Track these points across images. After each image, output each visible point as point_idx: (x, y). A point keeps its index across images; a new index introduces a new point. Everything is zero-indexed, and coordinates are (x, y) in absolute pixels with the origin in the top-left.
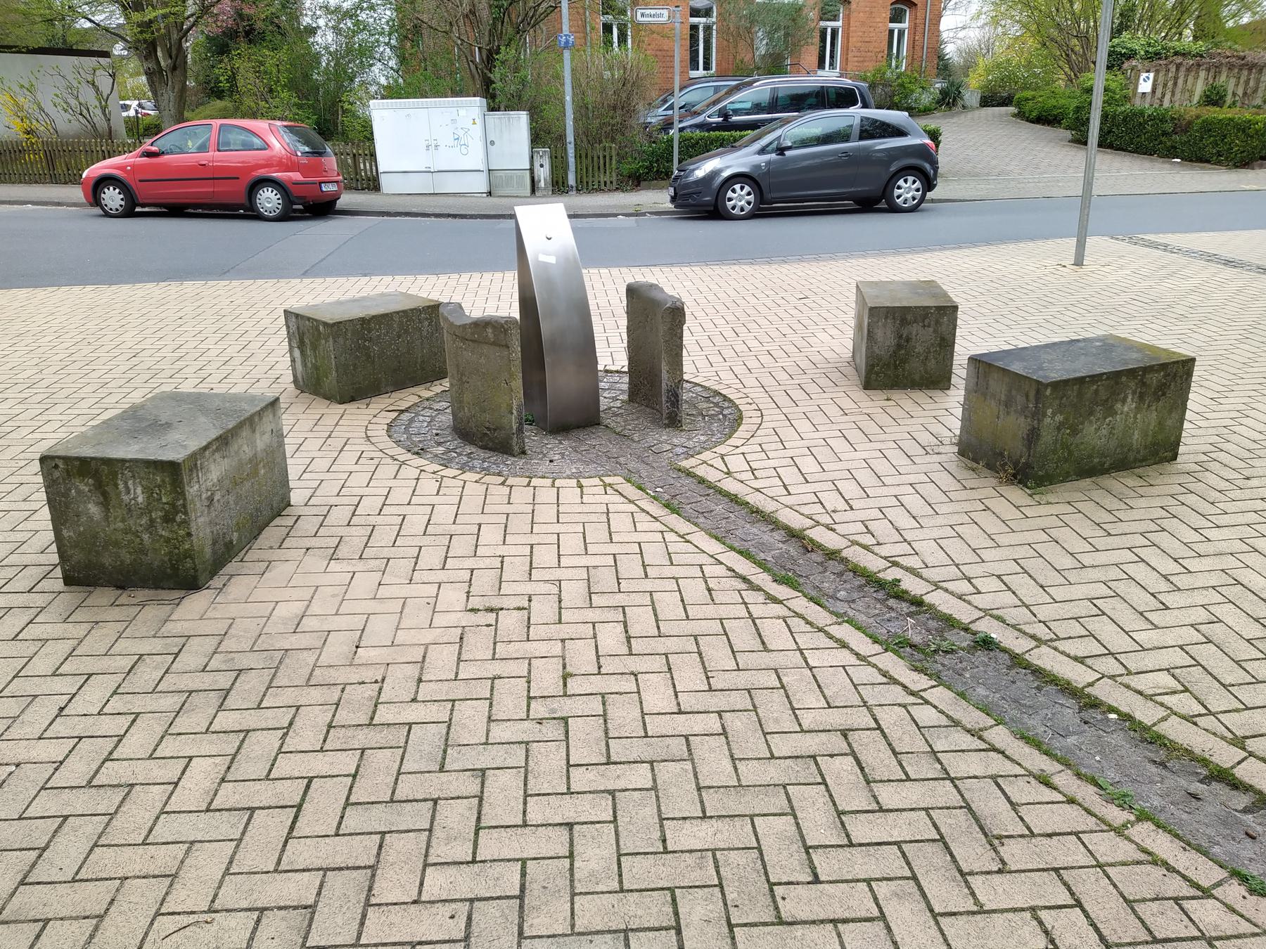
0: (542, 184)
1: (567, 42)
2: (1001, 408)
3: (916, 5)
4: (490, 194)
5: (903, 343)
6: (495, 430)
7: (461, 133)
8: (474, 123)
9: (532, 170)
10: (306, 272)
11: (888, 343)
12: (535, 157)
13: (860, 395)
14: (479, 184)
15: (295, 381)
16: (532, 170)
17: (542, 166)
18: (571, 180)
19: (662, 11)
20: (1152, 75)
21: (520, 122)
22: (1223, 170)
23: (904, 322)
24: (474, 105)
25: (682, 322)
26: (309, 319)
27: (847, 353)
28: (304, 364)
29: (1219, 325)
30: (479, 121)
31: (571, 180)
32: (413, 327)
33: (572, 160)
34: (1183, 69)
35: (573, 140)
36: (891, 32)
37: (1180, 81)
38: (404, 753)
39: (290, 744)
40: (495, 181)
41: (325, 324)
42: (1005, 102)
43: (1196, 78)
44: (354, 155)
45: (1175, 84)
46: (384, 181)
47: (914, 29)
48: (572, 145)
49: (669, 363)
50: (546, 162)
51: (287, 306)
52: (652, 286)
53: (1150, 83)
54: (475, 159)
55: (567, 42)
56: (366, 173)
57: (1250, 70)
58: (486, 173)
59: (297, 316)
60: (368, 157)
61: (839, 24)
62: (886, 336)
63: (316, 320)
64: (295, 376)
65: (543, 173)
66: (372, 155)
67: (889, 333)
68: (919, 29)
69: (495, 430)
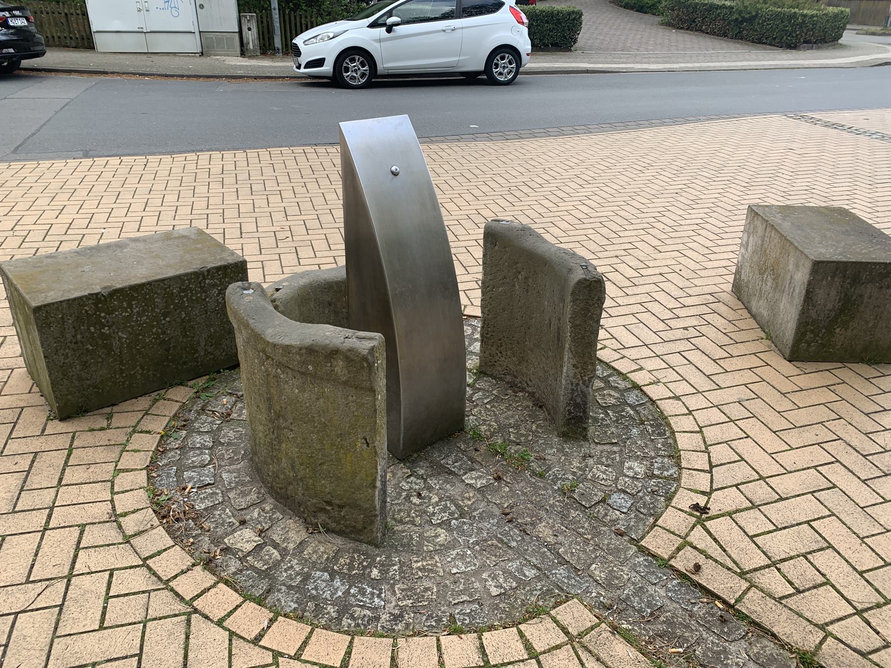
6: (341, 507)
10: (17, 148)
12: (243, 21)
13: (788, 368)
14: (192, 44)
17: (249, 29)
22: (780, 50)
23: (855, 280)
29: (703, 145)
32: (190, 300)
33: (277, 24)
44: (66, 14)
46: (97, 38)
48: (277, 11)
49: (575, 354)
50: (254, 25)
52: (525, 229)
56: (79, 31)
58: (197, 34)
60: (80, 17)
62: (828, 298)
65: (252, 36)
66: (84, 15)
67: (833, 293)
69: (341, 507)
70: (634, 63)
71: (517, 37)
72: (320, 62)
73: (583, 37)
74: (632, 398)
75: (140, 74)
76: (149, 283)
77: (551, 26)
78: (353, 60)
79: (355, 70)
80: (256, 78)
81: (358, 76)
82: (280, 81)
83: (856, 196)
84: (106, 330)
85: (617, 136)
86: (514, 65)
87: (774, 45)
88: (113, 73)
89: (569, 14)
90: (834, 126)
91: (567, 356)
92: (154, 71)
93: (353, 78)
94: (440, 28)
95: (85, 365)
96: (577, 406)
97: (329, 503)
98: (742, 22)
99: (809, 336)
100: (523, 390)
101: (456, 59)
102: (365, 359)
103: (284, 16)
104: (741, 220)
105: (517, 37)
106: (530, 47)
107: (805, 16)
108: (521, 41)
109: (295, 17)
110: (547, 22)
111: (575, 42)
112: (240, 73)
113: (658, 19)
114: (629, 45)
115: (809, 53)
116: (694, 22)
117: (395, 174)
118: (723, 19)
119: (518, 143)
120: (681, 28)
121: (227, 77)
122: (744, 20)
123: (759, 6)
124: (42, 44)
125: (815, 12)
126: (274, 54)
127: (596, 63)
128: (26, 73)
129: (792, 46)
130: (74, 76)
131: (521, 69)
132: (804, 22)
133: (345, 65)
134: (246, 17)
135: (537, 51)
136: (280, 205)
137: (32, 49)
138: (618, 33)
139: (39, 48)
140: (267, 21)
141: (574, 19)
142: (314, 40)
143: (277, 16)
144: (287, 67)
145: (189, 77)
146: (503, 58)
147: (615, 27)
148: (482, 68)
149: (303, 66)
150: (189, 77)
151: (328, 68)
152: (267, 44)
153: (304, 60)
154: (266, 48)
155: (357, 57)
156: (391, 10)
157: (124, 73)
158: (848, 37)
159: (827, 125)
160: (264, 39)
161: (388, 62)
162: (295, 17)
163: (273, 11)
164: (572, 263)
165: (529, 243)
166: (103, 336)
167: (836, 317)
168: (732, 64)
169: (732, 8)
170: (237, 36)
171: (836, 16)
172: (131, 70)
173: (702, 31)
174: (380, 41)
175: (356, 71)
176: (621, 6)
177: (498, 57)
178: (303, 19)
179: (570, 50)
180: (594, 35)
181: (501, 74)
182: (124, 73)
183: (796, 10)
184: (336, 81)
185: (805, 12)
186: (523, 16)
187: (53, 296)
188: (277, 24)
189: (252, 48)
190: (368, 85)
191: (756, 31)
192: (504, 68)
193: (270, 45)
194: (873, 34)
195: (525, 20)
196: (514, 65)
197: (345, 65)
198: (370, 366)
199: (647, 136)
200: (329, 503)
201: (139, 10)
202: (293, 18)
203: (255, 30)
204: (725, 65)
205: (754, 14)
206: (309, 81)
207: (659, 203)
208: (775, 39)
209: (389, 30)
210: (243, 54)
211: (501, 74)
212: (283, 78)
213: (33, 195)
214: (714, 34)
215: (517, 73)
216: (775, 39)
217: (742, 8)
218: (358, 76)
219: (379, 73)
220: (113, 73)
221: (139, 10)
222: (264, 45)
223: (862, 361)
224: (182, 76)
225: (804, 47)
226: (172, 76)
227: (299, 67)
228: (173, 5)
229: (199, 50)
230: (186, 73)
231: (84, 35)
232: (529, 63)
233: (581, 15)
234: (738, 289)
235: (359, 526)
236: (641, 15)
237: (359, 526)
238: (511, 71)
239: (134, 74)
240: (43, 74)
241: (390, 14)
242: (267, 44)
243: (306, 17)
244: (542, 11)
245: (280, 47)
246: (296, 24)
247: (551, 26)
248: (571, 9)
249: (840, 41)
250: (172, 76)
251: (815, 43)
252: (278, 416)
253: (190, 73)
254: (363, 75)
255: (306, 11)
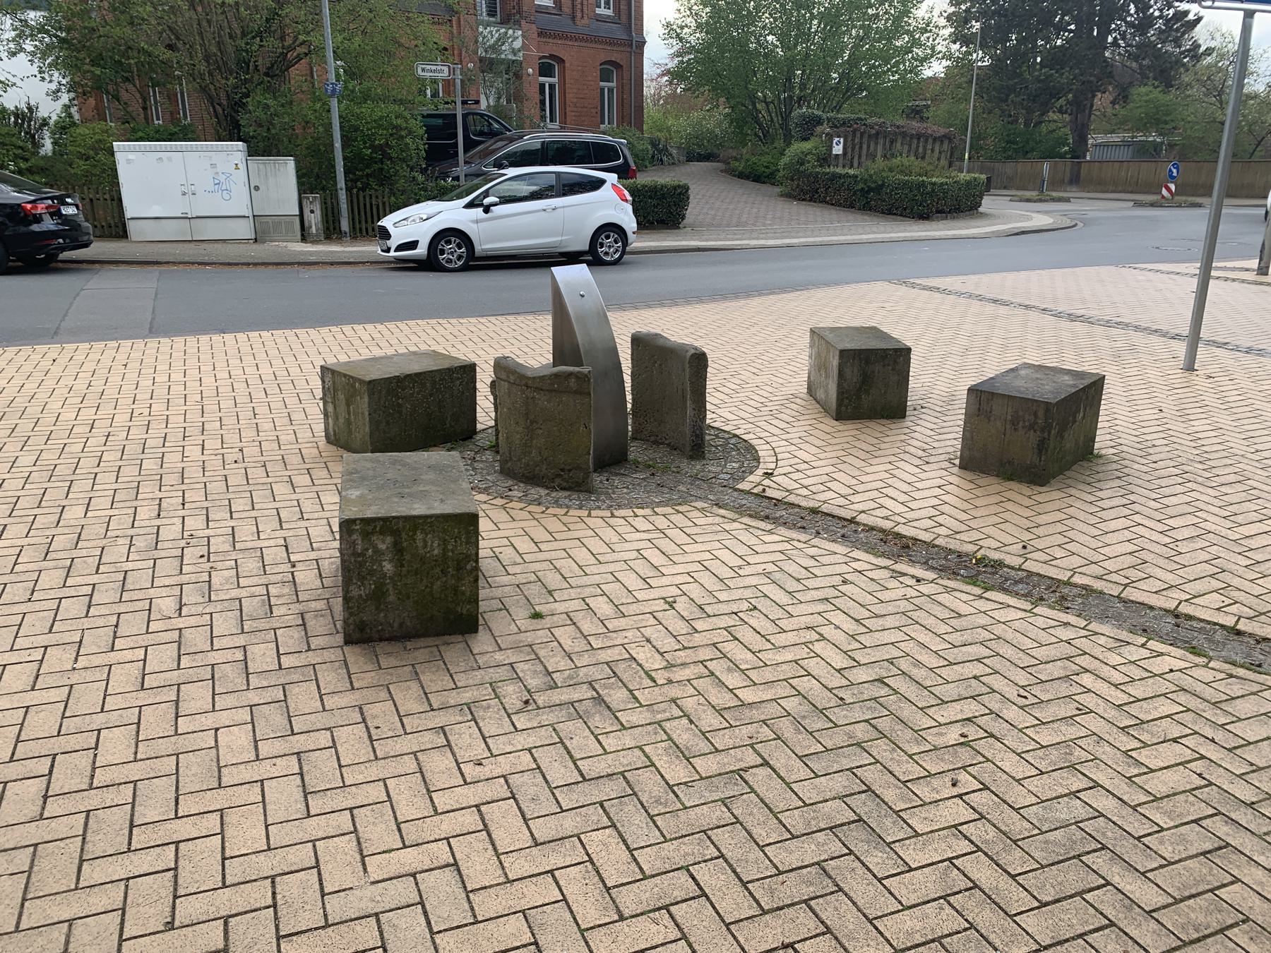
0: (314, 230)
1: (334, 90)
2: (1008, 426)
3: (622, 66)
4: (256, 240)
5: (866, 380)
6: (570, 471)
7: (222, 178)
8: (237, 168)
9: (301, 215)
11: (855, 380)
13: (836, 423)
14: (244, 230)
15: (327, 436)
16: (301, 215)
17: (312, 212)
18: (345, 225)
19: (443, 68)
20: (842, 140)
21: (288, 168)
22: (912, 222)
23: (868, 362)
24: (235, 151)
25: (706, 366)
26: (345, 376)
27: (799, 384)
28: (336, 418)
30: (242, 167)
31: (345, 225)
33: (344, 206)
34: (866, 136)
35: (344, 186)
36: (602, 90)
37: (865, 146)
38: (177, 778)
39: (40, 784)
40: (264, 228)
41: (361, 382)
42: (707, 157)
43: (876, 144)
44: (91, 200)
45: (861, 148)
46: (132, 227)
47: (621, 87)
48: (344, 192)
49: (694, 402)
50: (317, 207)
51: (1111, 390)
53: (841, 146)
54: (239, 205)
55: (334, 90)
57: (942, 142)
58: (251, 218)
59: (333, 372)
60: (109, 202)
61: (614, 84)
62: (853, 374)
63: (352, 377)
64: (326, 430)
65: (314, 219)
67: (856, 371)
68: (626, 88)
69: (570, 471)
70: (749, 239)
71: (622, 216)
72: (413, 245)
73: (693, 212)
74: (733, 441)
75: (200, 264)
76: (424, 373)
77: (655, 202)
78: (449, 242)
79: (451, 252)
80: (332, 264)
81: (454, 258)
82: (361, 267)
83: (1117, 422)
84: (400, 401)
85: (727, 304)
86: (620, 244)
87: (905, 216)
88: (167, 263)
89: (675, 188)
90: (930, 289)
91: (689, 403)
92: (215, 260)
93: (449, 261)
94: (540, 208)
95: (388, 423)
96: (697, 436)
97: (562, 470)
98: (868, 192)
99: (846, 401)
100: (663, 443)
101: (560, 238)
102: (586, 376)
103: (351, 196)
104: (807, 339)
105: (622, 216)
106: (635, 225)
107: (934, 184)
108: (626, 219)
109: (364, 197)
110: (650, 197)
111: (683, 218)
112: (313, 259)
113: (777, 190)
114: (744, 220)
115: (942, 224)
116: (817, 193)
117: (582, 296)
118: (848, 189)
119: (635, 313)
120: (803, 200)
121: (299, 264)
122: (870, 190)
123: (884, 174)
124: (89, 234)
125: (944, 180)
126: (340, 238)
127: (707, 240)
128: (66, 266)
129: (924, 216)
130: (122, 267)
131: (628, 249)
132: (933, 190)
133: (440, 247)
134: (308, 198)
135: (647, 228)
136: (259, 459)
137: (80, 239)
138: (731, 207)
139: (86, 238)
140: (332, 203)
141: (680, 194)
142: (405, 222)
143: (344, 197)
144: (373, 252)
145: (255, 264)
146: (608, 237)
147: (728, 200)
148: (587, 248)
149: (392, 250)
150: (255, 264)
151: (421, 250)
152: (332, 228)
153: (393, 243)
154: (331, 231)
155: (453, 239)
156: (487, 191)
157: (180, 263)
158: (987, 204)
159: (925, 288)
160: (327, 222)
161: (486, 244)
162: (364, 197)
163: (340, 191)
164: (688, 348)
165: (661, 342)
166: (400, 406)
167: (860, 388)
168: (857, 238)
169: (857, 177)
170: (297, 220)
171: (968, 183)
172: (187, 259)
173: (827, 203)
174: (477, 222)
175: (452, 253)
176: (734, 176)
177: (603, 236)
178: (374, 199)
179: (679, 228)
180: (705, 210)
181: (607, 254)
182: (180, 263)
183: (925, 178)
184: (430, 264)
185: (934, 180)
186: (626, 193)
187: (374, 377)
188: (344, 206)
189: (314, 231)
190: (465, 268)
191: (885, 201)
192: (610, 247)
193: (334, 229)
194: (1028, 200)
195: (629, 198)
196: (620, 244)
197: (440, 247)
198: (589, 380)
199: (756, 303)
200: (562, 470)
201: (184, 194)
202: (361, 199)
203: (318, 212)
204: (849, 238)
205: (880, 183)
206: (392, 265)
207: (760, 348)
208: (905, 209)
209: (487, 210)
210: (304, 239)
211: (607, 254)
212: (364, 263)
213: (9, 422)
214: (840, 205)
215: (624, 253)
216: (905, 209)
217: (866, 177)
218: (454, 258)
219: (477, 254)
220: (167, 263)
221: (184, 194)
222: (328, 229)
223: (883, 417)
224: (248, 264)
225: (937, 218)
226: (237, 264)
227: (388, 250)
228: (224, 188)
229: (253, 237)
230: (251, 261)
231: (112, 222)
232: (636, 243)
233: (688, 189)
234: (811, 390)
235: (580, 481)
236: (758, 185)
237: (580, 481)
238: (617, 251)
239: (193, 263)
240: (85, 266)
241: (486, 194)
242: (332, 228)
243: (377, 197)
244: (644, 186)
245: (347, 230)
246: (365, 205)
247: (655, 202)
248: (676, 183)
249: (980, 209)
250: (237, 264)
251: (949, 212)
252: (532, 422)
253: (256, 261)
254: (460, 258)
255: (376, 190)
